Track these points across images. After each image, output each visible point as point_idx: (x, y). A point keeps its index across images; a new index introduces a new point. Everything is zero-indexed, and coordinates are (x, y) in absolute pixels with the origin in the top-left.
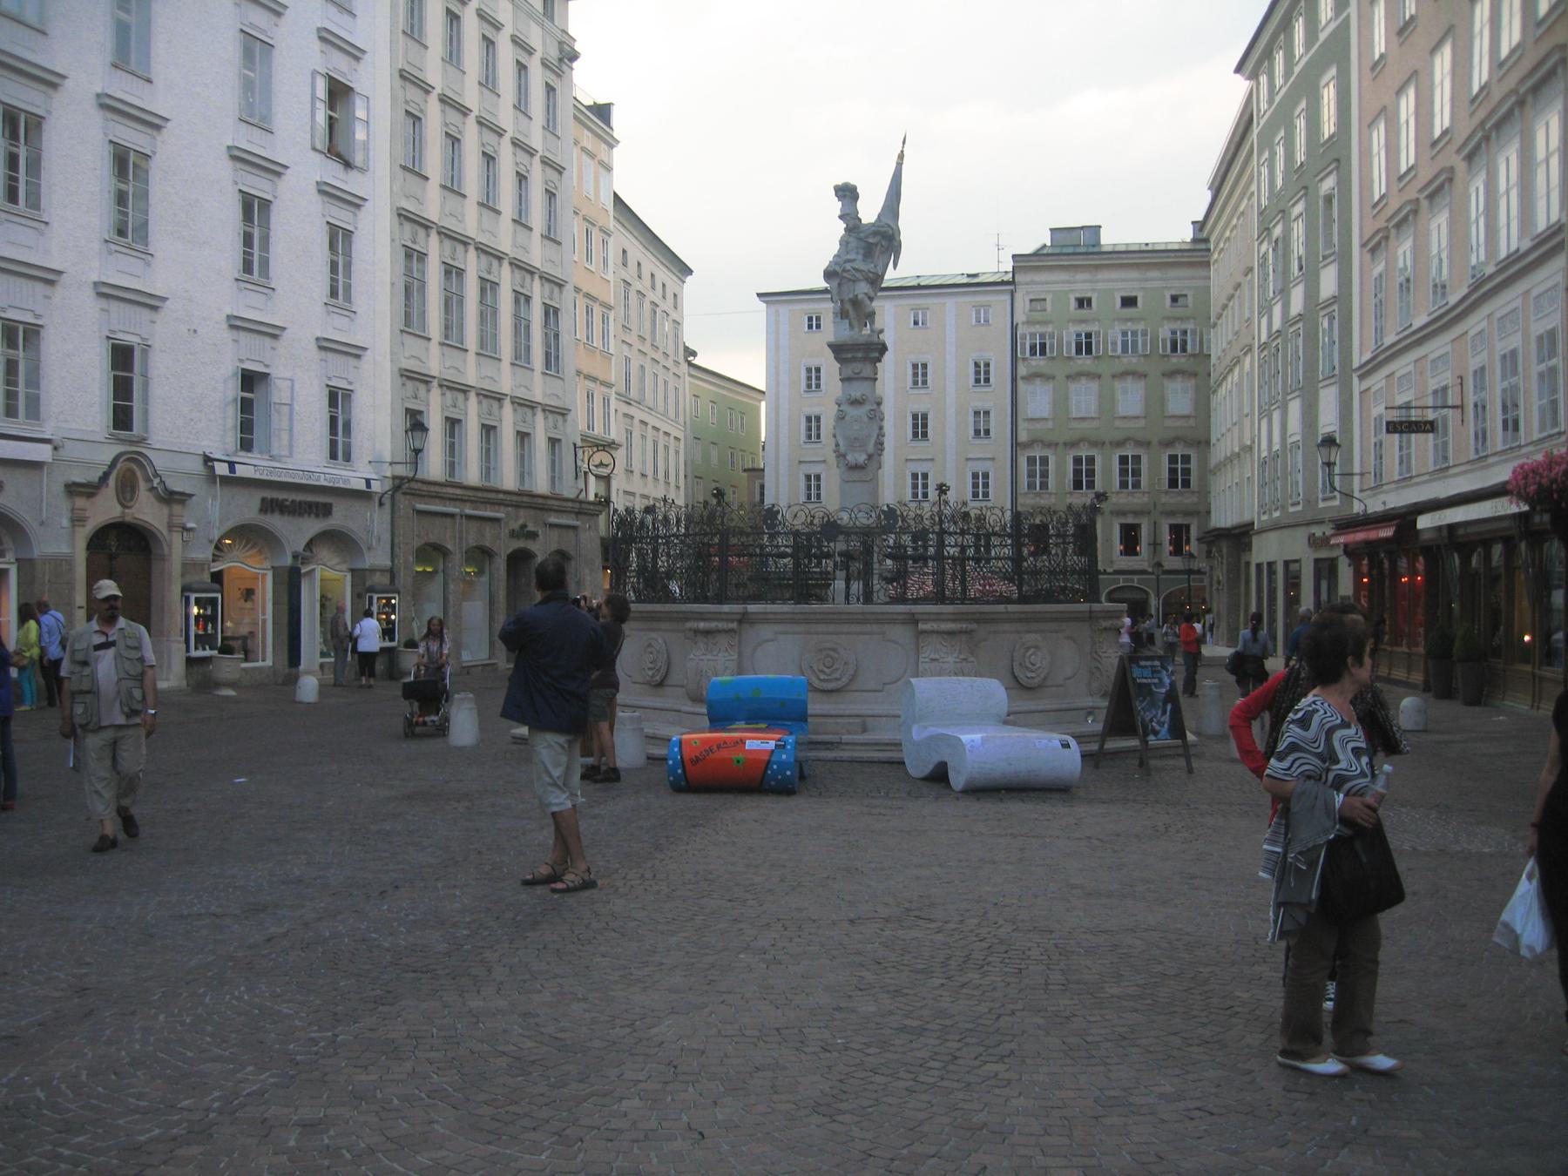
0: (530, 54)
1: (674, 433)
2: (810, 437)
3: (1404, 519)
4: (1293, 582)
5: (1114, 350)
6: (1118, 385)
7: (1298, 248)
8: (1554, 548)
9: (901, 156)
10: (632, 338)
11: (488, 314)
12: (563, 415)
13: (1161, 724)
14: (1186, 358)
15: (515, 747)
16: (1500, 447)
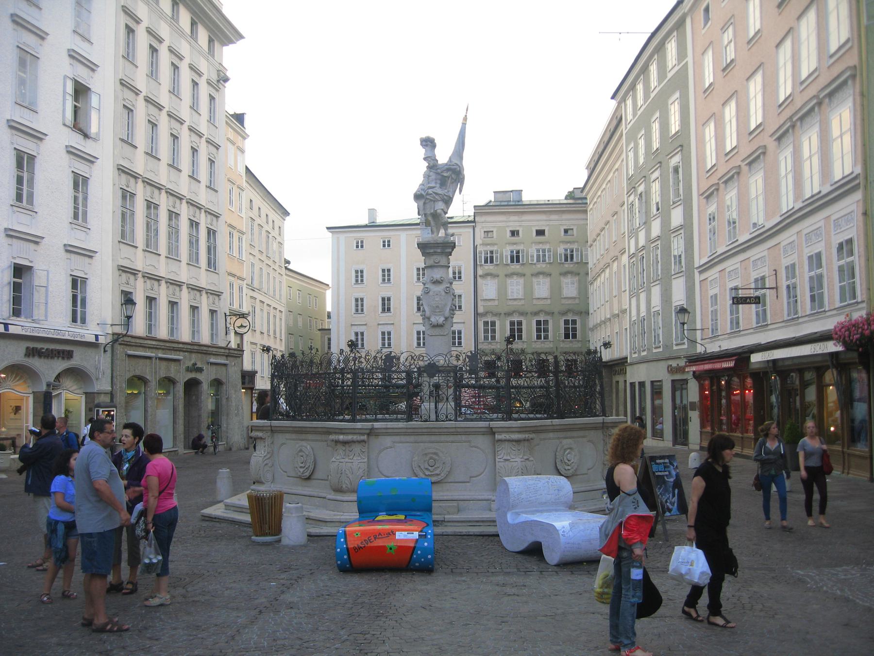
0: (200, 76)
1: (279, 308)
3: (742, 356)
5: (533, 260)
6: (535, 280)
7: (656, 196)
9: (465, 119)
10: (255, 252)
11: (174, 232)
12: (219, 296)
13: (673, 504)
14: (573, 263)
15: (205, 524)
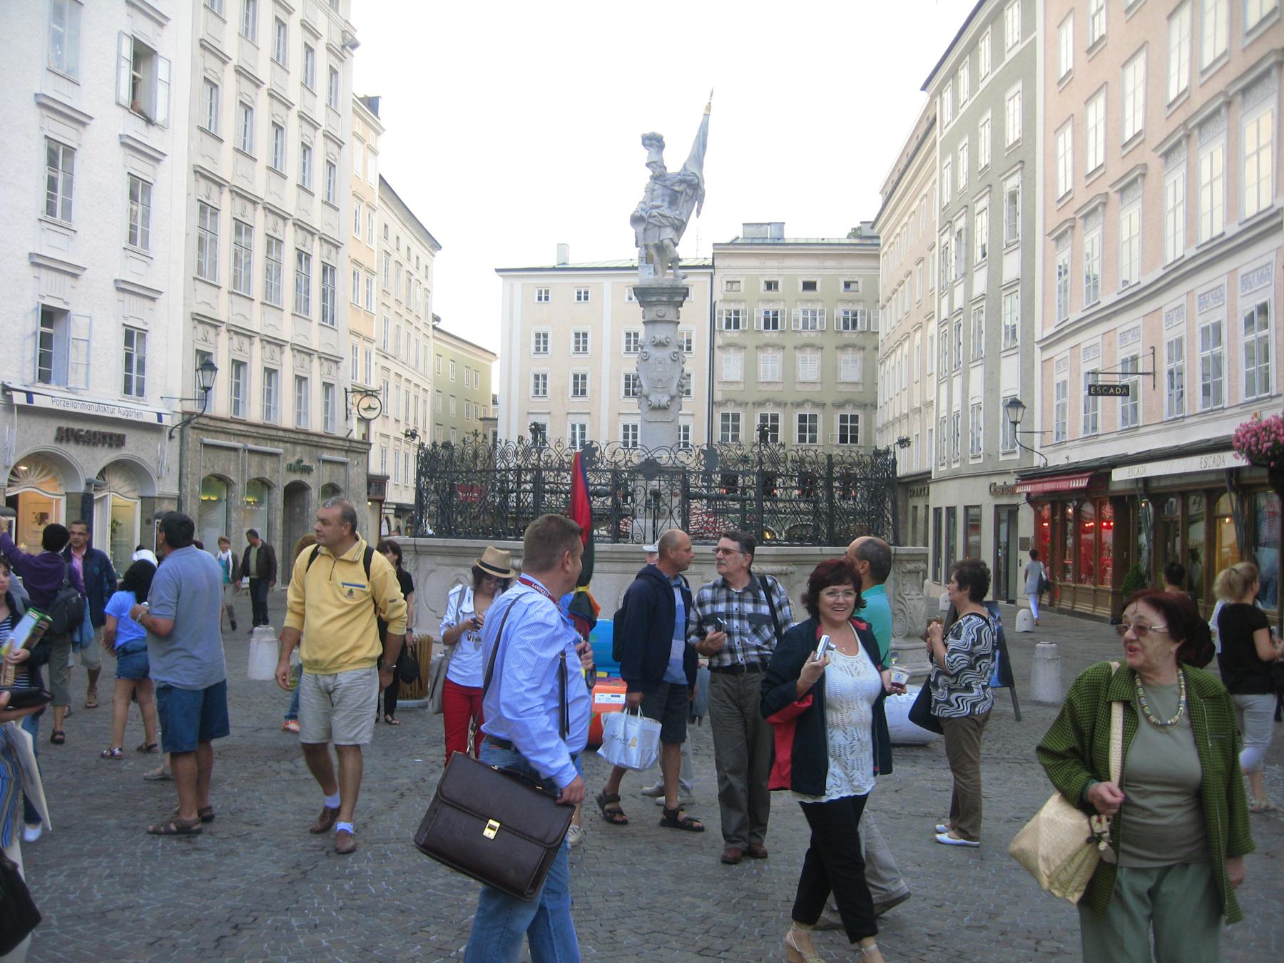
0: (317, 38)
1: (423, 385)
2: (537, 392)
3: (1099, 472)
4: (973, 525)
5: (796, 326)
6: (799, 355)
8: (1269, 502)
9: (709, 108)
12: (337, 362)
14: (856, 332)
16: (1199, 409)
